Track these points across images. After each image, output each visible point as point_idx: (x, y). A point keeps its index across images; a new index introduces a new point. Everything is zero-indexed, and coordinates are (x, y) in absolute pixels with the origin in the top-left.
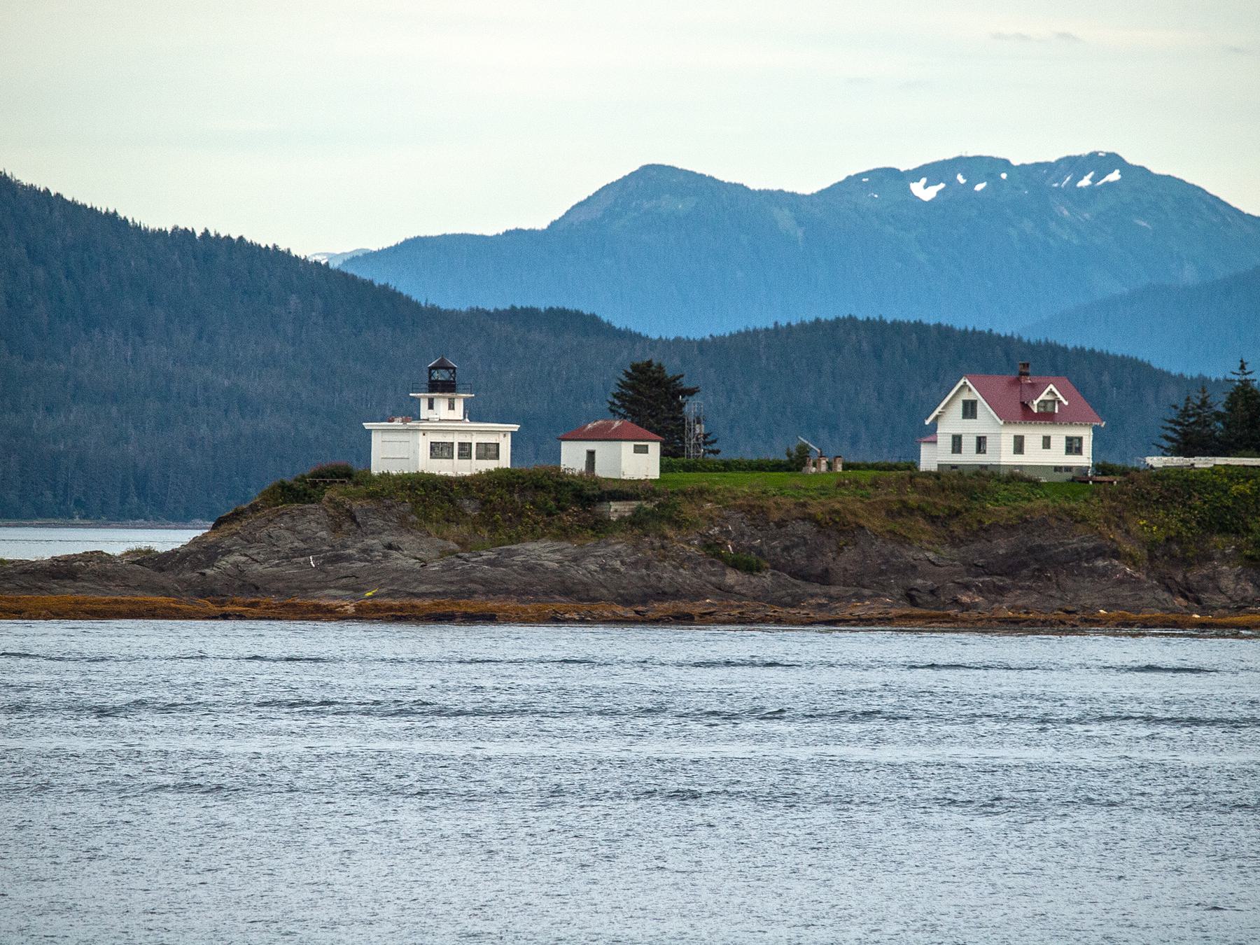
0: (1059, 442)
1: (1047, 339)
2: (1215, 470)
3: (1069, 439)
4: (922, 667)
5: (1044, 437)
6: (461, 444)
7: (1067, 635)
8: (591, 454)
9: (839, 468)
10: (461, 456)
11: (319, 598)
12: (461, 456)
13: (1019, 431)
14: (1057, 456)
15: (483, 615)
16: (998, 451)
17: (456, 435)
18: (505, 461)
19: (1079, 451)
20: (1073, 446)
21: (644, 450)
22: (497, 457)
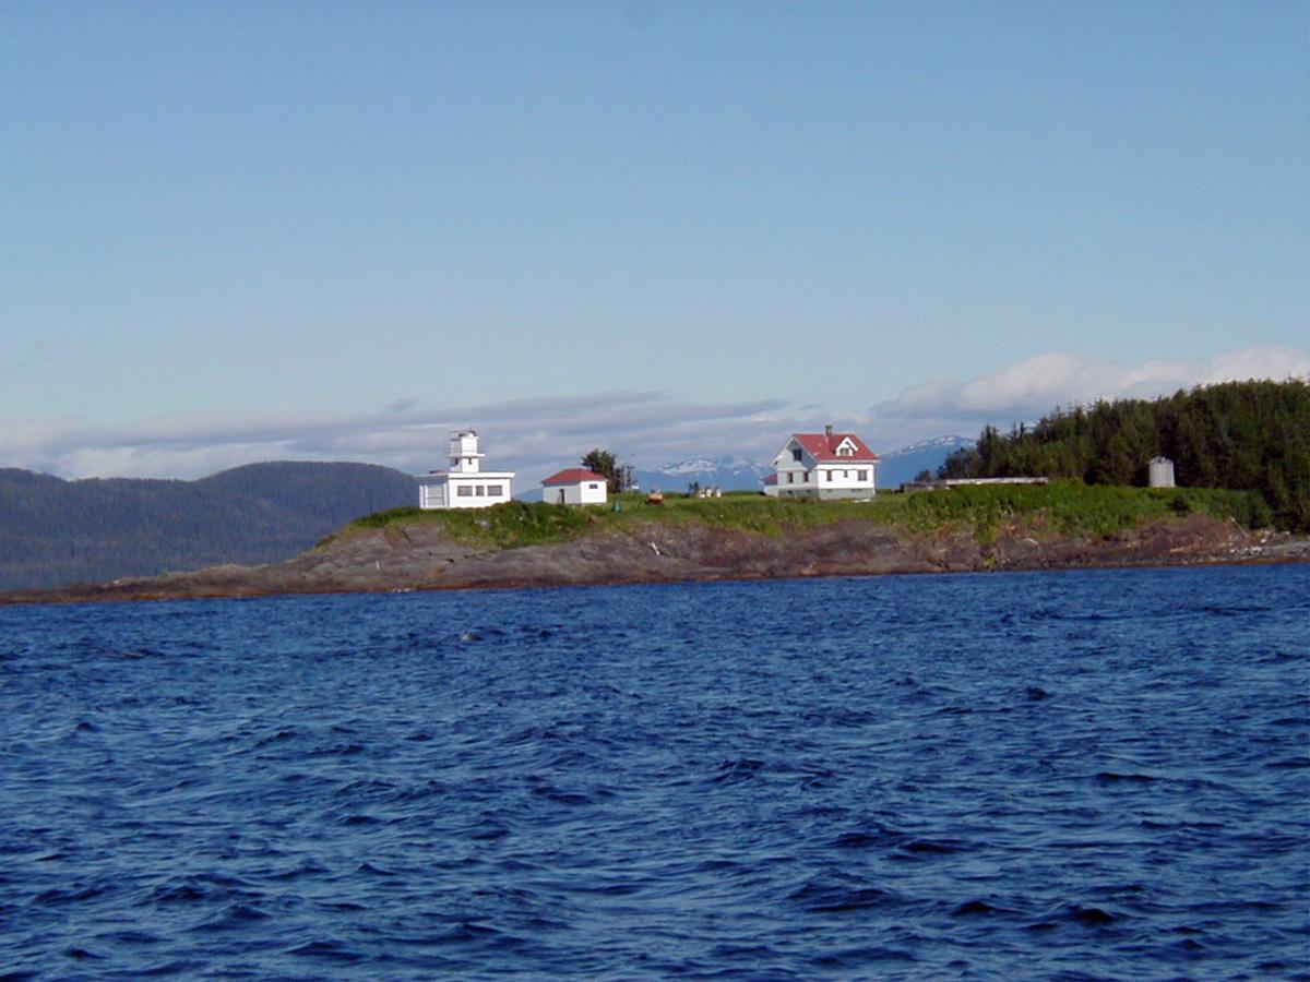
0: (853, 475)
1: (1076, 401)
2: (984, 485)
3: (860, 472)
4: (1123, 777)
5: (459, 494)
6: (477, 487)
7: (1201, 672)
8: (562, 491)
9: (719, 495)
10: (478, 494)
11: (306, 720)
12: (478, 494)
13: (561, 487)
14: (852, 482)
15: (1113, 937)
16: (817, 481)
17: (486, 481)
18: (505, 498)
19: (865, 479)
20: (862, 476)
21: (595, 487)
22: (500, 494)
